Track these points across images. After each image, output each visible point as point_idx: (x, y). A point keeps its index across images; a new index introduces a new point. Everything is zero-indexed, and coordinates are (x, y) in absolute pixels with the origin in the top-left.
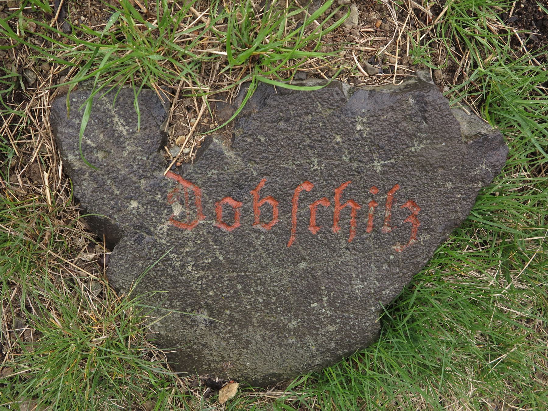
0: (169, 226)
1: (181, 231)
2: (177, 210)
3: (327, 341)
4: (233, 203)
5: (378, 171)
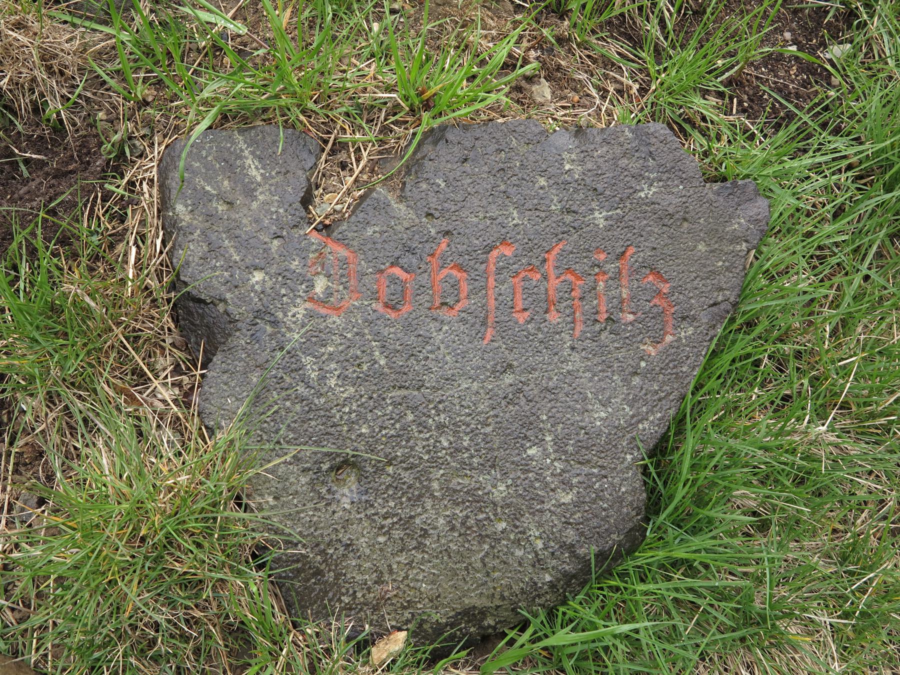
0: (306, 309)
1: (325, 318)
2: (320, 285)
3: (560, 526)
4: (403, 275)
5: (601, 226)
